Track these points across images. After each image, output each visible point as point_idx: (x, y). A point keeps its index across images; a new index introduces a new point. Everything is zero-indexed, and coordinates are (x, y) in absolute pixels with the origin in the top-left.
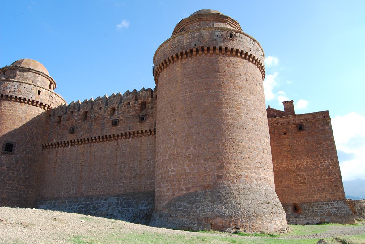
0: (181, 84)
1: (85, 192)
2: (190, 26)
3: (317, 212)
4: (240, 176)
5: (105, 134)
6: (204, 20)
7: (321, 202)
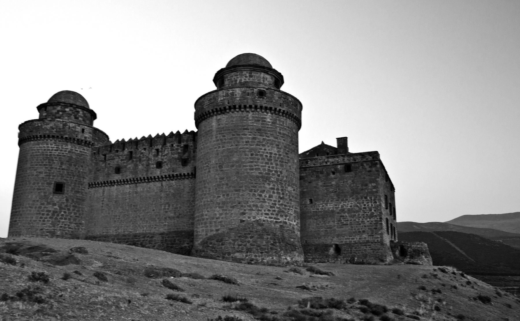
5: (150, 175)
6: (242, 71)
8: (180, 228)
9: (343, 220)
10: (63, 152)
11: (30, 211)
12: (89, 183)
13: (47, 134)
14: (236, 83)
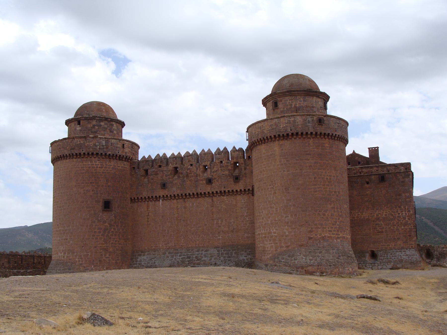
0: (279, 163)
1: (184, 244)
2: (283, 99)
3: (391, 258)
4: (324, 237)
5: (199, 191)
6: (296, 95)
7: (395, 249)
9: (378, 228)
10: (107, 169)
12: (131, 198)
13: (91, 151)
14: (291, 107)
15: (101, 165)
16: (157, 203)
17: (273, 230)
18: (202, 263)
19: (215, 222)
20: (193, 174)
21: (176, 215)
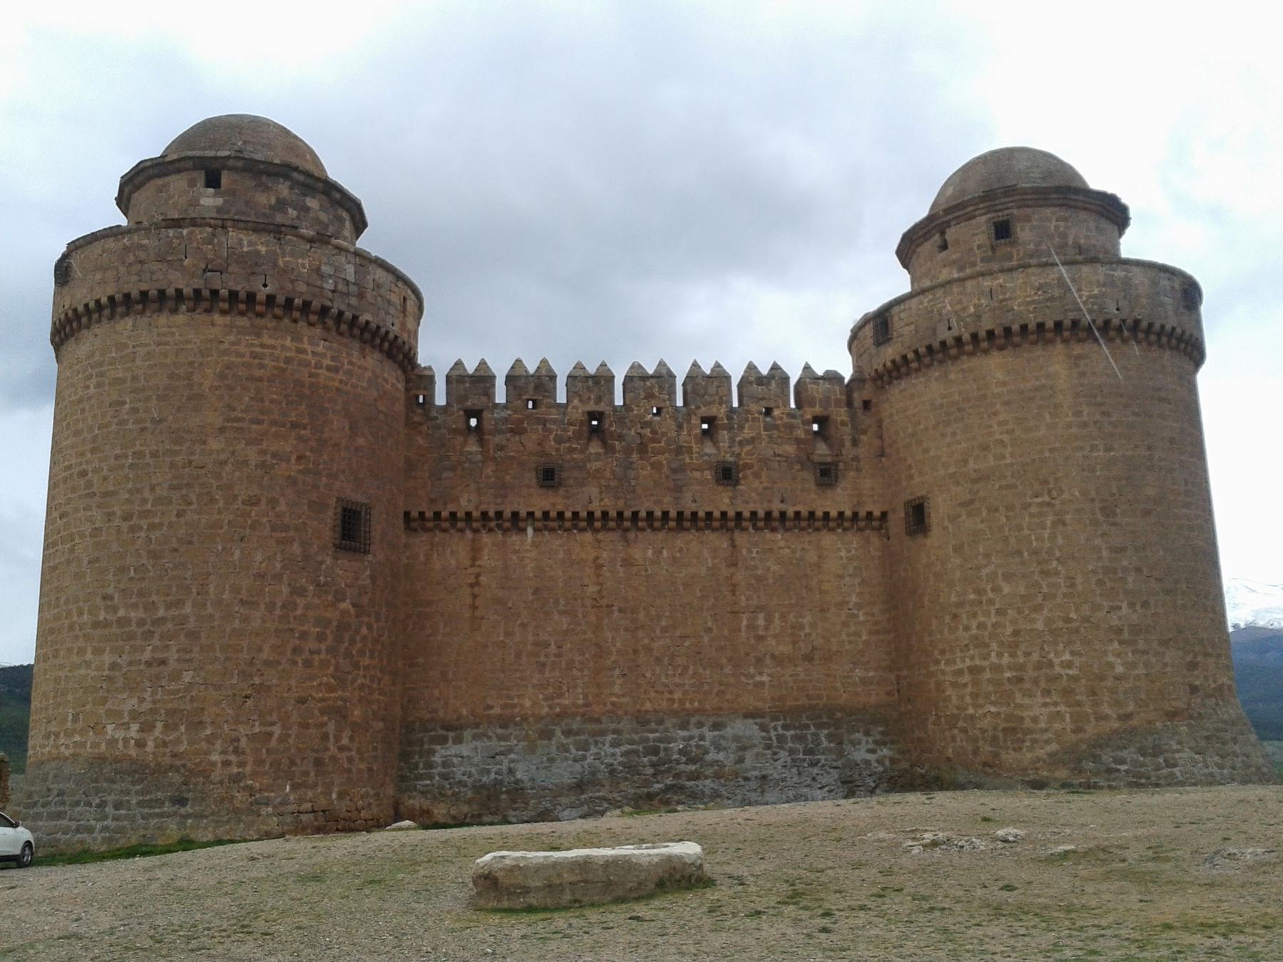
1: (624, 700)
5: (689, 506)
8: (820, 697)
11: (245, 619)
12: (407, 514)
15: (333, 359)
16: (515, 538)
17: (1057, 654)
18: (709, 772)
19: (745, 622)
20: (663, 444)
21: (592, 589)
